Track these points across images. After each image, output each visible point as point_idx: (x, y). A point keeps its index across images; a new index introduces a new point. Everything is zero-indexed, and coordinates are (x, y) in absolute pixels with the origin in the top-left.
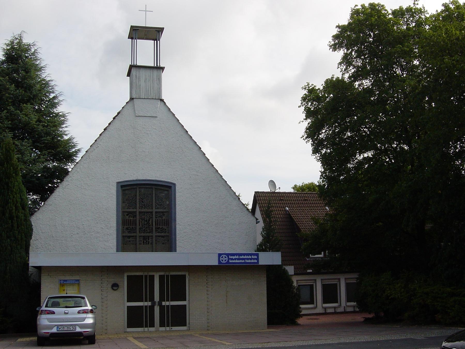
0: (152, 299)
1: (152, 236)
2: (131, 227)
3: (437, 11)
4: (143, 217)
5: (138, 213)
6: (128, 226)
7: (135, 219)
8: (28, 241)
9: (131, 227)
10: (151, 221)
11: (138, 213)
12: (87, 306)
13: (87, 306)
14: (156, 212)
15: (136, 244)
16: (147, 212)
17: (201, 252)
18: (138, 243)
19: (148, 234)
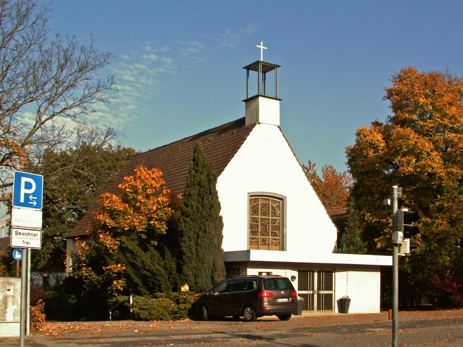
0: (319, 295)
1: (269, 239)
2: (254, 230)
3: (389, 107)
4: (263, 222)
5: (259, 219)
6: (252, 230)
7: (257, 223)
8: (148, 270)
9: (254, 230)
10: (267, 226)
11: (259, 219)
12: (263, 49)
13: (263, 49)
14: (272, 219)
15: (258, 245)
16: (265, 219)
17: (276, 272)
18: (259, 244)
19: (266, 237)
